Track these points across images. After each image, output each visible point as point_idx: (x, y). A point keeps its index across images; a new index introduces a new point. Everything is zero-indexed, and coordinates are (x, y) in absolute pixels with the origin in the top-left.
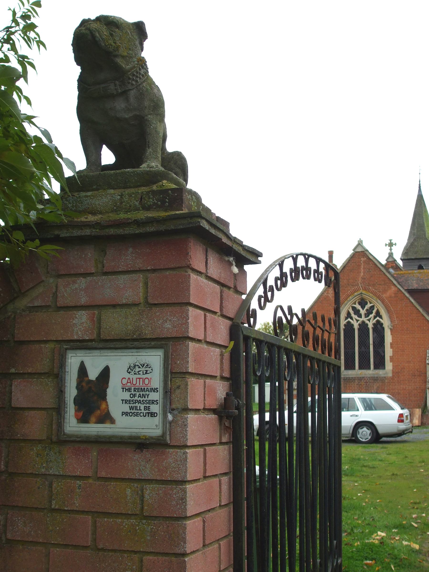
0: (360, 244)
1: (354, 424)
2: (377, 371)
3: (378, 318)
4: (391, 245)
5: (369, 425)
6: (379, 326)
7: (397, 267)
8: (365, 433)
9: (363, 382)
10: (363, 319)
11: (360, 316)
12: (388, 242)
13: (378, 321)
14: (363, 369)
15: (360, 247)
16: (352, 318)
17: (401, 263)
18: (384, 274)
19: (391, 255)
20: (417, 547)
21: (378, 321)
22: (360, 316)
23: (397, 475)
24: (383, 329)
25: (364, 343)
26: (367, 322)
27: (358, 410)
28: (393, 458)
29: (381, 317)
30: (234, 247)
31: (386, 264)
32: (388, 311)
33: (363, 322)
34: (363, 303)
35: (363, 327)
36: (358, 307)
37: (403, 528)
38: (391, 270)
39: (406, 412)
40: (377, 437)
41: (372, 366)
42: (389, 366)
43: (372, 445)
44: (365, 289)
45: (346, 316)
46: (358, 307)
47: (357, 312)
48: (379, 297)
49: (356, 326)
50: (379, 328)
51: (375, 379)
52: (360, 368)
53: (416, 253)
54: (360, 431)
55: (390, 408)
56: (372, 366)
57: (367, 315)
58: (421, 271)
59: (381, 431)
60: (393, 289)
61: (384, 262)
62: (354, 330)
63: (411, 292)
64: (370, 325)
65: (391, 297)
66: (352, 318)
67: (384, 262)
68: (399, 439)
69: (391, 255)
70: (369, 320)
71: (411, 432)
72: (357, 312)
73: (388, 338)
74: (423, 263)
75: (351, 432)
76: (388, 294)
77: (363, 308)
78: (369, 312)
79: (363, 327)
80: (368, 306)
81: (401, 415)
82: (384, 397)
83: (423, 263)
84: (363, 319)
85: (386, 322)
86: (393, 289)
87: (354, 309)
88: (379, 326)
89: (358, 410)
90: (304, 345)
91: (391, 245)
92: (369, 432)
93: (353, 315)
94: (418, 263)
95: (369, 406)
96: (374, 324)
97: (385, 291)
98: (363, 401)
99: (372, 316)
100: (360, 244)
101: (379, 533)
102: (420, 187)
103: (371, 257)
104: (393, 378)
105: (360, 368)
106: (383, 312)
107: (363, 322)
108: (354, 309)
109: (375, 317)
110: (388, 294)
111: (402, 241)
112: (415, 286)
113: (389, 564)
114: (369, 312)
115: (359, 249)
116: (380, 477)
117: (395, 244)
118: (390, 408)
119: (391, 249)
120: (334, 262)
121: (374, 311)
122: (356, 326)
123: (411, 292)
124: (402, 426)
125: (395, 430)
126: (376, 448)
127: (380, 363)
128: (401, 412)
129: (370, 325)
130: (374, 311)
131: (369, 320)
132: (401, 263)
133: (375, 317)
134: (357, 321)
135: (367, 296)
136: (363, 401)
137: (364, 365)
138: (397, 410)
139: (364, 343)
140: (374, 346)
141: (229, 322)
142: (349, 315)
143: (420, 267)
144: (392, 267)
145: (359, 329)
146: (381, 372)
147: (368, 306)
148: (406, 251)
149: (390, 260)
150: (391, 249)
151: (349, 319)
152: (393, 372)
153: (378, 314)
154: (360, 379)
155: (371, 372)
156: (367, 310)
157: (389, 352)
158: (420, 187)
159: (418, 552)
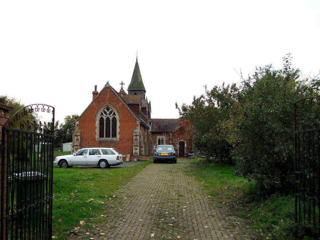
0: (108, 83)
1: (98, 160)
2: (113, 138)
3: (114, 116)
4: (122, 84)
5: (105, 160)
6: (114, 119)
7: (124, 94)
8: (103, 164)
9: (107, 143)
10: (108, 116)
11: (107, 114)
12: (121, 83)
13: (114, 117)
14: (108, 137)
15: (107, 85)
16: (103, 115)
17: (127, 92)
18: (117, 97)
19: (122, 88)
20: (103, 203)
21: (114, 117)
22: (107, 114)
23: (110, 180)
24: (116, 120)
25: (108, 126)
26: (110, 117)
27: (101, 155)
28: (111, 174)
29: (115, 115)
30: (3, 107)
31: (120, 92)
32: (119, 113)
33: (108, 117)
34: (108, 109)
35: (108, 119)
36: (106, 111)
37: (101, 197)
38: (122, 95)
39: (120, 155)
40: (109, 166)
41: (111, 136)
42: (118, 136)
43: (105, 169)
44: (109, 103)
45: (165, 105)
46: (106, 111)
47: (105, 113)
48: (115, 107)
49: (105, 119)
50: (114, 120)
51: (112, 142)
52: (106, 137)
53: (134, 88)
54: (101, 163)
55: (114, 154)
56: (111, 136)
57: (110, 114)
58: (136, 96)
59: (110, 163)
60: (121, 103)
61: (118, 91)
62: (104, 120)
63: (130, 105)
64: (111, 119)
65: (120, 107)
66: (103, 115)
67: (118, 91)
68: (118, 166)
69: (122, 88)
70: (110, 116)
71: (122, 164)
72: (105, 113)
73: (118, 124)
74: (136, 92)
75: (97, 164)
76: (119, 105)
77: (108, 111)
78: (110, 113)
79: (108, 119)
80: (111, 110)
81: (118, 157)
82: (111, 149)
83: (136, 92)
84: (108, 116)
85: (117, 117)
86: (121, 103)
87: (104, 111)
88: (114, 119)
89: (101, 155)
90: (28, 130)
91: (122, 84)
92: (105, 163)
93: (104, 114)
94: (135, 92)
95: (105, 153)
96: (112, 118)
97: (118, 104)
98: (102, 150)
99: (111, 115)
100: (108, 83)
101: (91, 199)
102: (137, 59)
103: (112, 89)
104: (119, 141)
105: (106, 137)
106: (116, 113)
107: (108, 117)
108: (104, 111)
109: (113, 115)
110: (119, 105)
111: (128, 82)
112: (131, 102)
113: (89, 208)
114: (110, 113)
115: (107, 86)
116: (103, 181)
117: (124, 84)
118: (114, 154)
119: (122, 86)
120: (97, 90)
121: (113, 113)
122: (105, 119)
123: (130, 105)
124: (118, 161)
125: (115, 163)
126: (107, 171)
127: (114, 135)
128: (119, 155)
129: (111, 119)
130: (113, 113)
131: (110, 116)
132: (127, 92)
133: (113, 115)
134: (105, 116)
135: (110, 106)
136: (102, 150)
137: (108, 136)
138: (117, 154)
139: (108, 126)
140: (112, 128)
141: (2, 126)
142: (102, 114)
143: (136, 94)
144: (122, 94)
145: (106, 120)
146: (114, 139)
147: (111, 110)
148: (130, 87)
149: (122, 90)
150: (122, 86)
151: (102, 116)
152: (120, 139)
153: (114, 114)
154: (106, 141)
155: (111, 139)
156: (110, 112)
157: (118, 130)
158: (137, 59)
159: (103, 204)
